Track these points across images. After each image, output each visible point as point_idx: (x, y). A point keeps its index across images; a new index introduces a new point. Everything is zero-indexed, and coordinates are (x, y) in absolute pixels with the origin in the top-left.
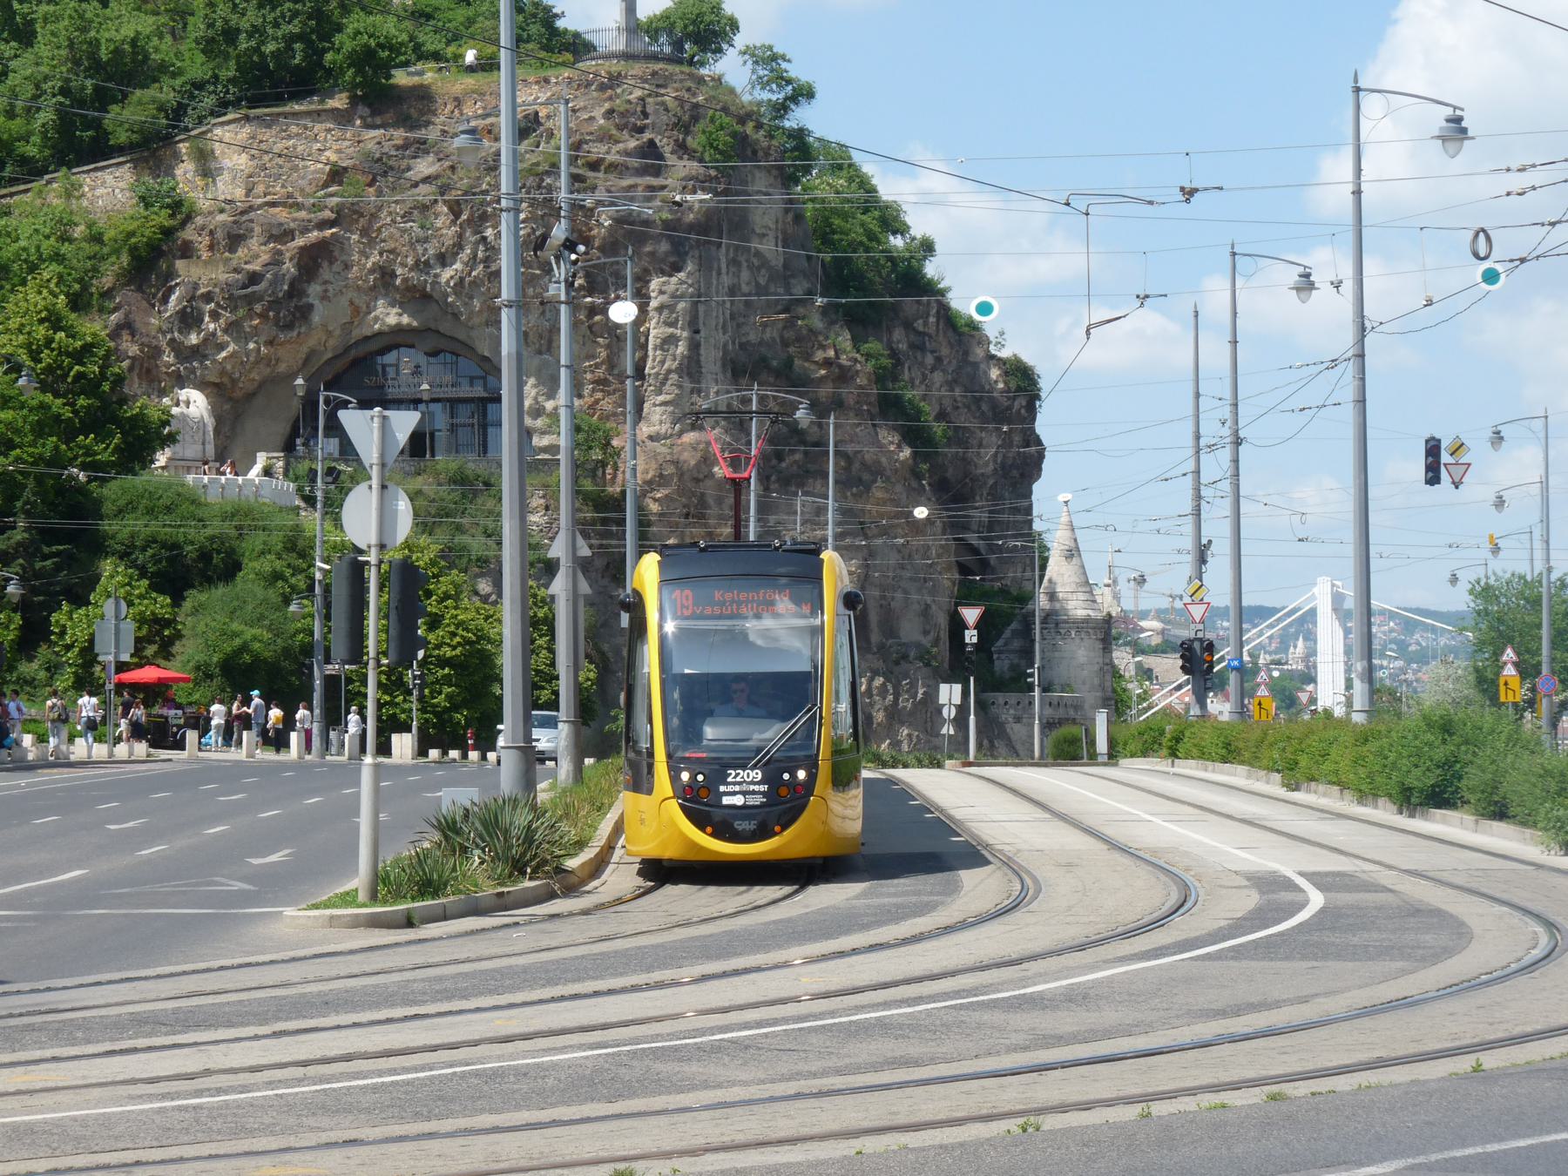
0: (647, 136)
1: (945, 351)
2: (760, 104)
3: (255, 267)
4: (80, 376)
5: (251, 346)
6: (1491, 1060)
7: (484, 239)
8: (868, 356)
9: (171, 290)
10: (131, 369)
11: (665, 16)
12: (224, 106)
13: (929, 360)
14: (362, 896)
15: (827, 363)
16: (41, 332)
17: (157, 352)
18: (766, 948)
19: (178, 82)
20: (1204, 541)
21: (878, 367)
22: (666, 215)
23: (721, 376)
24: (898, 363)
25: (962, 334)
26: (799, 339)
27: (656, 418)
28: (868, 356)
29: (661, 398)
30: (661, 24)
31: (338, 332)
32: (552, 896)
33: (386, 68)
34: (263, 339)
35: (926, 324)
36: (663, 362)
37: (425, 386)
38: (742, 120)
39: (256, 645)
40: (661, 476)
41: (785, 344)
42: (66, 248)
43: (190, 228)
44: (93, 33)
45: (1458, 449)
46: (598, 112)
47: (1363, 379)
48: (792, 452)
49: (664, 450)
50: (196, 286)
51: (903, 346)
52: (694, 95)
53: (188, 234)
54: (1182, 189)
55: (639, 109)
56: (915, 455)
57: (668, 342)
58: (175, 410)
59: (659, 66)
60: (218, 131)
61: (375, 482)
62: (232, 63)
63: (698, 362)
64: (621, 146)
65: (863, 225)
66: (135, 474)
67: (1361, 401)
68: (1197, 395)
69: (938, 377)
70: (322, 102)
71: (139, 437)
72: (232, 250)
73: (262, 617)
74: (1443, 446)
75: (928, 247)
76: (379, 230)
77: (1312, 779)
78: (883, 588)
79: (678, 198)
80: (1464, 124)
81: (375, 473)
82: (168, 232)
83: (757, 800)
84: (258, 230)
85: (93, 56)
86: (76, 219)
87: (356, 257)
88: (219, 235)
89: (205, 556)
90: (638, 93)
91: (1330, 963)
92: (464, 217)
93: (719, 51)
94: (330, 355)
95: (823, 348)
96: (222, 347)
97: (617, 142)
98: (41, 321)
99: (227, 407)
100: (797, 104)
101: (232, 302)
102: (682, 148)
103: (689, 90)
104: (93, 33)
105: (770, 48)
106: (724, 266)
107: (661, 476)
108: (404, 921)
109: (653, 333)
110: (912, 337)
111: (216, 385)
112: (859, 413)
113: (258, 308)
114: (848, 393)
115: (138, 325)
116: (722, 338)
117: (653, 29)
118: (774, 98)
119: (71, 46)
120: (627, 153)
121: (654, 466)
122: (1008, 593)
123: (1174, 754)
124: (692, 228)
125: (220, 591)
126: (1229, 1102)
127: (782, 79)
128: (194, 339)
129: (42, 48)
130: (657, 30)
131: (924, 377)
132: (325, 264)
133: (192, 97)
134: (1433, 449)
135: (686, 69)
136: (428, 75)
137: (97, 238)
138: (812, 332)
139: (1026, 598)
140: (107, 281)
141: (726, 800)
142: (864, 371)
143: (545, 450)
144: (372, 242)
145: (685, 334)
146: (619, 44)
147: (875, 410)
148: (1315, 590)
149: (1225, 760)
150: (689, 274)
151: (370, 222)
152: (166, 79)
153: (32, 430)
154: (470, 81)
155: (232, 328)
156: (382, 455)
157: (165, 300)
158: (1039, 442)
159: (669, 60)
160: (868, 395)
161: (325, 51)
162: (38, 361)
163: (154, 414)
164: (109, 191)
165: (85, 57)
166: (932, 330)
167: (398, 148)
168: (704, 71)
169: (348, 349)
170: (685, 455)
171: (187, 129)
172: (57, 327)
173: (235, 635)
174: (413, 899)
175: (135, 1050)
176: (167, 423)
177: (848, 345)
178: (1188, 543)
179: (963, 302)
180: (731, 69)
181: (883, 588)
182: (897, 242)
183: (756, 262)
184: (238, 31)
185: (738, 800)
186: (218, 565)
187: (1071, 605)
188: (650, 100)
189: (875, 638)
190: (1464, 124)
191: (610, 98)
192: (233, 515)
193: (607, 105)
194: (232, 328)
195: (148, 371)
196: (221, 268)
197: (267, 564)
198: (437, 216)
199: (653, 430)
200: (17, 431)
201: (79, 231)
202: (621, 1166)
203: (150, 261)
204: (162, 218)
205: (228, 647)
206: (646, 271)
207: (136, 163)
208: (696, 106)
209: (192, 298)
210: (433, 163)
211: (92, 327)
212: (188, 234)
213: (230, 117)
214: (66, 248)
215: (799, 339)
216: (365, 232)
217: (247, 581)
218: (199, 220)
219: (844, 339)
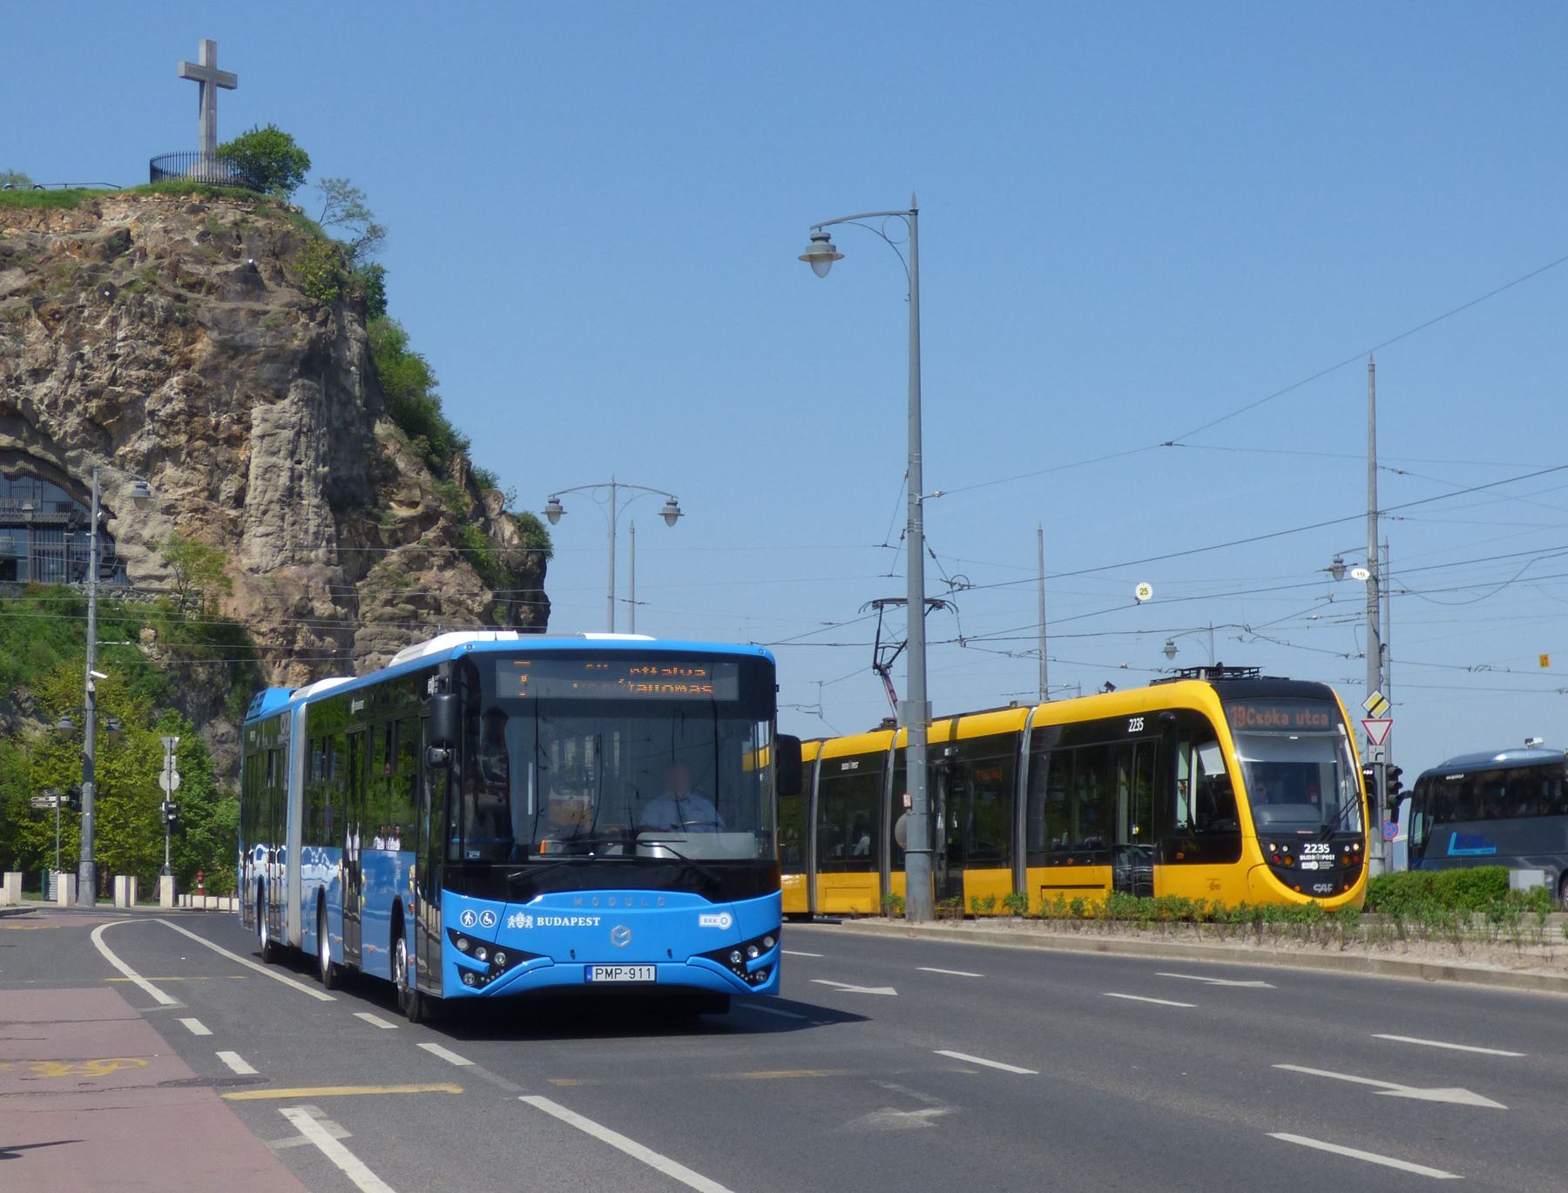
7: (81, 357)
29: (262, 530)
46: (192, 236)
55: (234, 233)
68: (1374, 467)
83: (1328, 866)
102: (278, 274)
109: (254, 462)
141: (1304, 866)
158: (545, 598)
180: (306, 198)
185: (1314, 866)
193: (200, 228)
198: (30, 330)
210: (20, 277)
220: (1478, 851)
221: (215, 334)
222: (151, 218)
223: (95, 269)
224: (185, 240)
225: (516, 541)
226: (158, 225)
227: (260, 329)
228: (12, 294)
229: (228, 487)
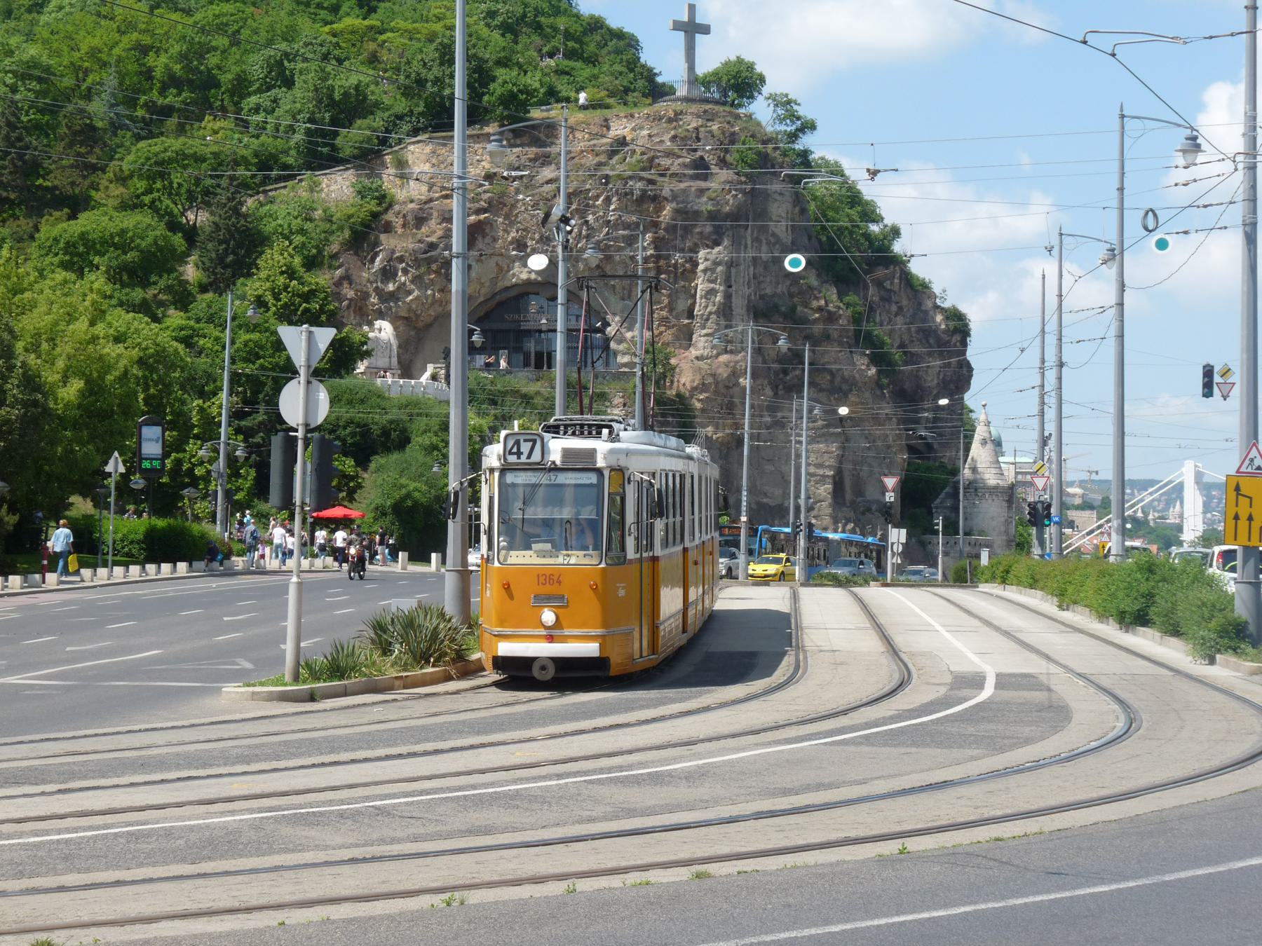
0: (699, 153)
1: (905, 302)
2: (778, 133)
3: (433, 239)
4: (306, 310)
5: (429, 292)
6: (914, 844)
7: (587, 222)
8: (848, 305)
9: (376, 254)
10: (349, 307)
11: (716, 73)
12: (415, 132)
13: (894, 308)
14: (288, 677)
15: (820, 309)
16: (281, 280)
17: (366, 296)
18: (486, 733)
19: (387, 114)
20: (1046, 434)
21: (854, 313)
22: (710, 208)
23: (746, 317)
24: (871, 309)
25: (917, 290)
26: (800, 293)
27: (701, 345)
28: (848, 305)
29: (704, 332)
30: (712, 78)
31: (487, 284)
32: (448, 678)
33: (524, 107)
34: (437, 288)
35: (892, 283)
36: (706, 307)
37: (544, 321)
38: (764, 142)
39: (417, 494)
40: (703, 384)
41: (791, 296)
42: (308, 225)
43: (391, 212)
44: (330, 82)
45: (1226, 372)
46: (666, 137)
47: (1122, 321)
48: (794, 369)
49: (707, 367)
50: (393, 252)
51: (876, 299)
52: (732, 126)
53: (390, 216)
54: (868, 170)
56: (879, 372)
57: (710, 293)
58: (371, 335)
59: (708, 107)
60: (411, 148)
61: (302, 378)
62: (422, 103)
63: (730, 307)
64: (681, 160)
65: (848, 216)
66: (341, 377)
67: (1121, 336)
69: (899, 320)
70: (481, 128)
71: (346, 353)
72: (418, 227)
73: (422, 475)
74: (1216, 370)
75: (895, 232)
76: (516, 216)
77: (1075, 603)
78: (855, 463)
79: (505, 174)
80: (1198, 141)
81: (302, 371)
82: (375, 215)
84: (435, 214)
85: (330, 97)
86: (314, 205)
87: (501, 233)
88: (410, 218)
89: (386, 433)
90: (694, 125)
91: (920, 750)
92: (574, 207)
93: (752, 97)
94: (482, 299)
95: (817, 299)
96: (409, 293)
97: (679, 157)
98: (282, 273)
99: (412, 333)
100: (804, 133)
101: (417, 263)
102: (723, 163)
103: (729, 123)
104: (330, 82)
105: (786, 95)
106: (749, 243)
107: (703, 384)
108: (308, 697)
110: (882, 293)
111: (406, 318)
112: (841, 344)
113: (434, 267)
114: (833, 329)
115: (354, 277)
116: (747, 291)
117: (706, 82)
118: (789, 129)
119: (316, 90)
120: (685, 165)
121: (698, 377)
122: (945, 467)
123: (1004, 581)
124: (728, 216)
125: (395, 456)
126: (653, 880)
127: (793, 116)
128: (391, 287)
129: (297, 92)
130: (709, 82)
131: (890, 320)
132: (480, 238)
133: (395, 125)
134: (1208, 372)
135: (727, 108)
136: (555, 112)
137: (329, 219)
138: (810, 288)
139: (955, 472)
140: (335, 248)
142: (845, 314)
143: (625, 365)
144: (512, 224)
145: (722, 288)
146: (682, 91)
147: (852, 341)
148: (1183, 470)
149: (1031, 587)
150: (725, 248)
151: (511, 209)
152: (379, 113)
153: (272, 347)
154: (581, 116)
155: (417, 280)
156: (308, 359)
157: (373, 261)
159: (717, 102)
160: (848, 331)
161: (483, 94)
162: (279, 300)
163: (357, 338)
164: (338, 187)
165: (325, 98)
166: (896, 288)
167: (530, 160)
168: (742, 111)
169: (495, 295)
170: (720, 371)
171: (391, 147)
172: (291, 277)
173: (403, 486)
174: (325, 681)
175: (221, 776)
176: (366, 343)
177: (835, 297)
178: (1035, 435)
179: (917, 268)
180: (761, 110)
181: (855, 463)
182: (875, 228)
183: (772, 240)
184: (426, 81)
186: (393, 439)
187: (987, 476)
188: (702, 129)
189: (849, 496)
190: (1198, 141)
191: (675, 128)
192: (407, 406)
193: (673, 133)
194: (417, 280)
195: (361, 308)
196: (410, 240)
197: (427, 440)
199: (698, 353)
200: (262, 347)
201: (318, 214)
202: (42, 937)
203: (364, 234)
204: (373, 206)
205: (397, 495)
206: (696, 245)
207: (357, 168)
208: (733, 134)
209: (391, 260)
211: (322, 279)
212: (390, 216)
213: (419, 138)
214: (308, 225)
215: (800, 293)
216: (507, 217)
217: (413, 451)
218: (397, 208)
219: (833, 293)
220: (32, 840)
221: (674, 205)
222: (642, 128)
223: (600, 164)
224: (662, 141)
225: (943, 327)
226: (645, 132)
227: (705, 199)
228: (547, 182)
229: (682, 305)
